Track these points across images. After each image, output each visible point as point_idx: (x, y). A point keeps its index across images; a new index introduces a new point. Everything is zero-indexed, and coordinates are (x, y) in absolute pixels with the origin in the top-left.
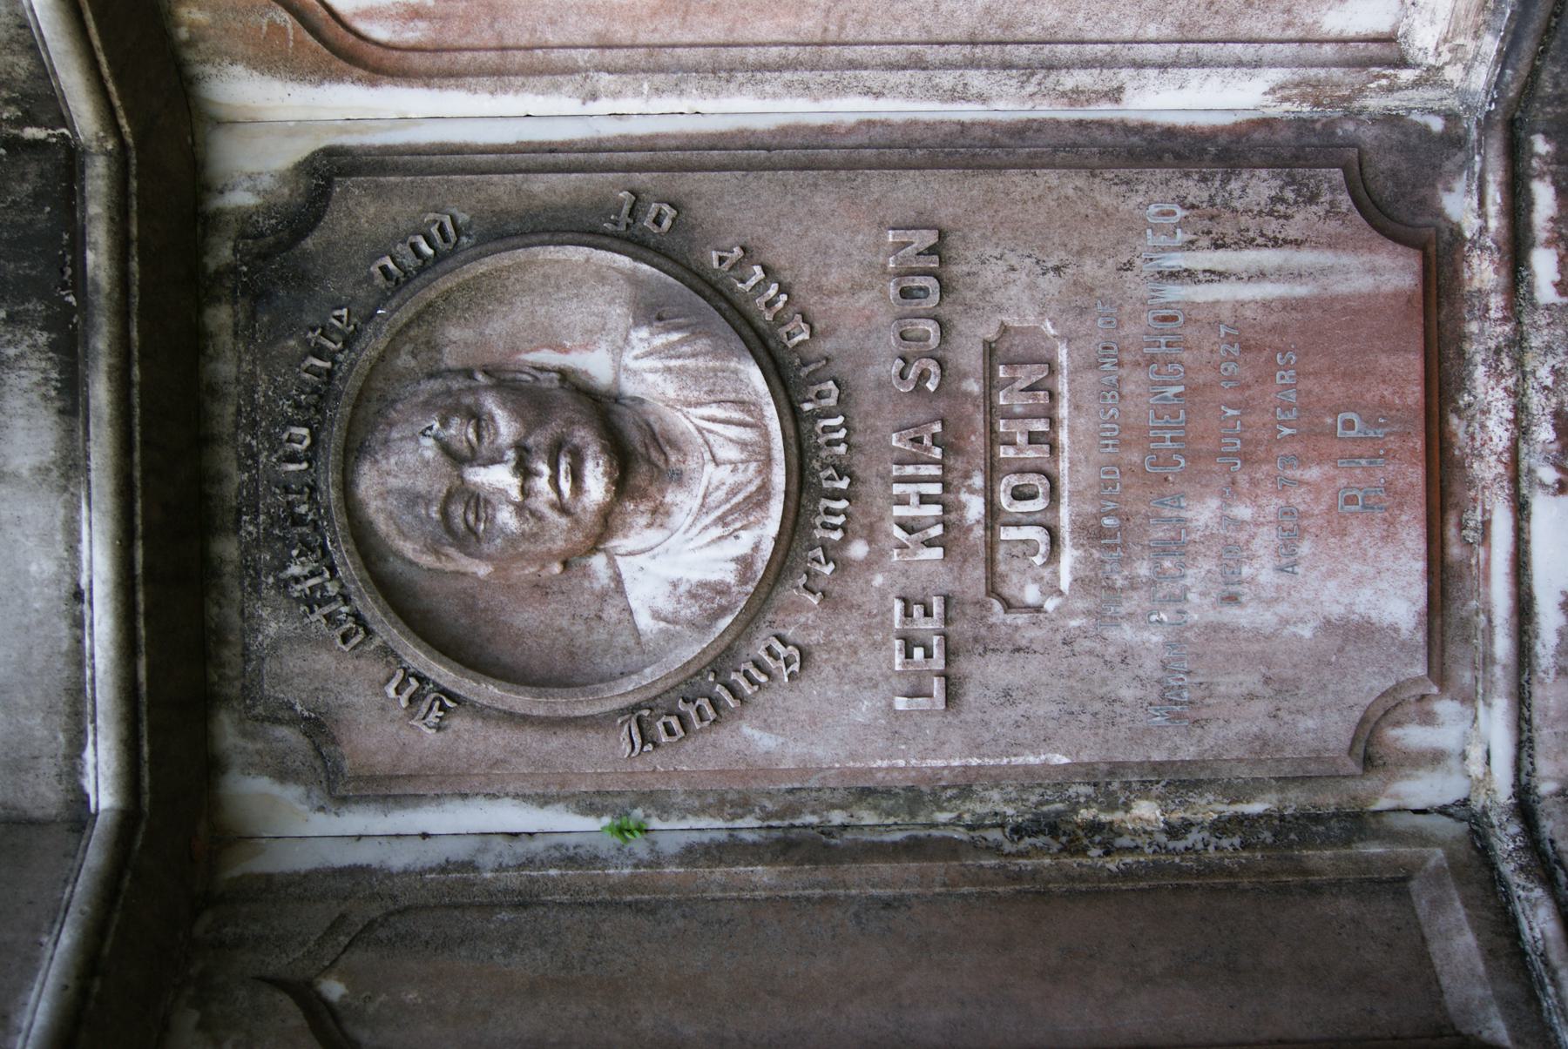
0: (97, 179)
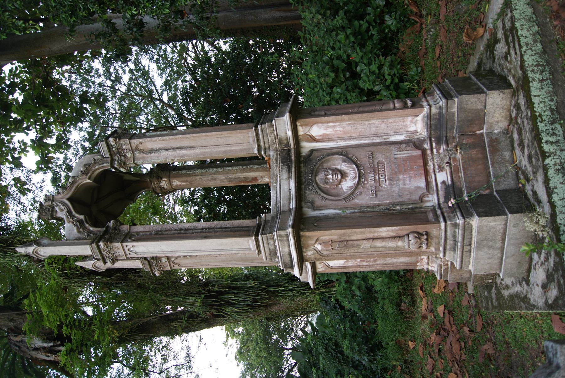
0: (293, 151)
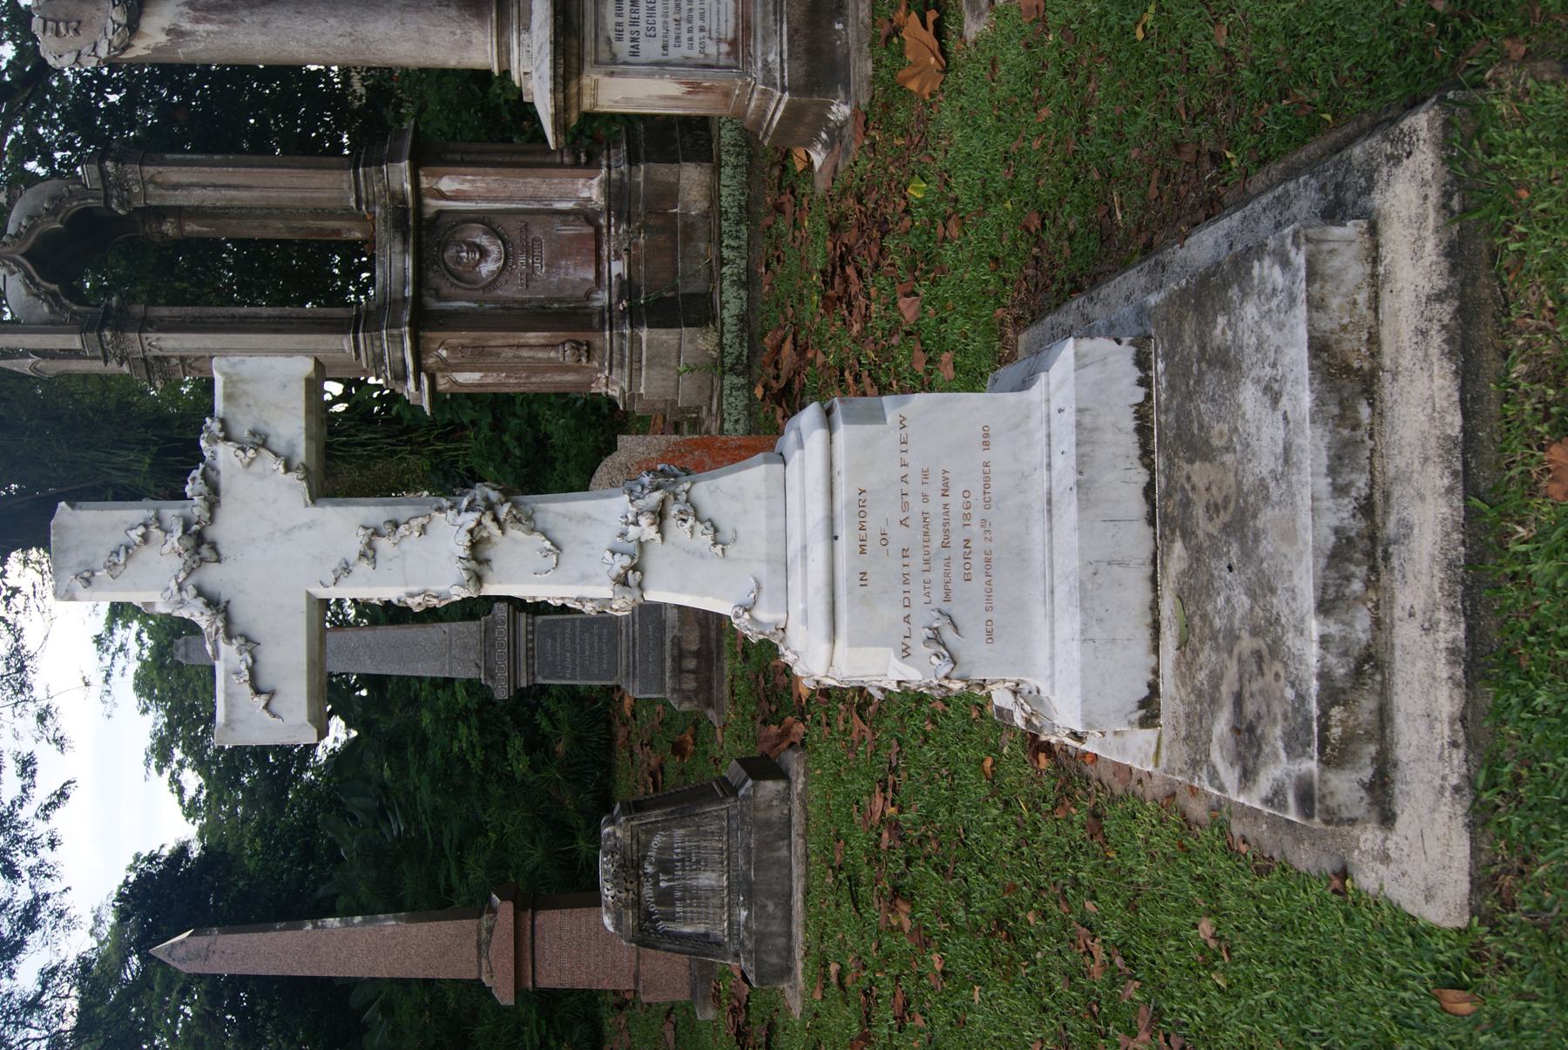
0: (411, 212)
